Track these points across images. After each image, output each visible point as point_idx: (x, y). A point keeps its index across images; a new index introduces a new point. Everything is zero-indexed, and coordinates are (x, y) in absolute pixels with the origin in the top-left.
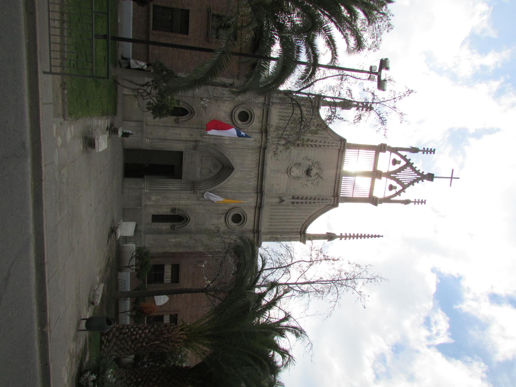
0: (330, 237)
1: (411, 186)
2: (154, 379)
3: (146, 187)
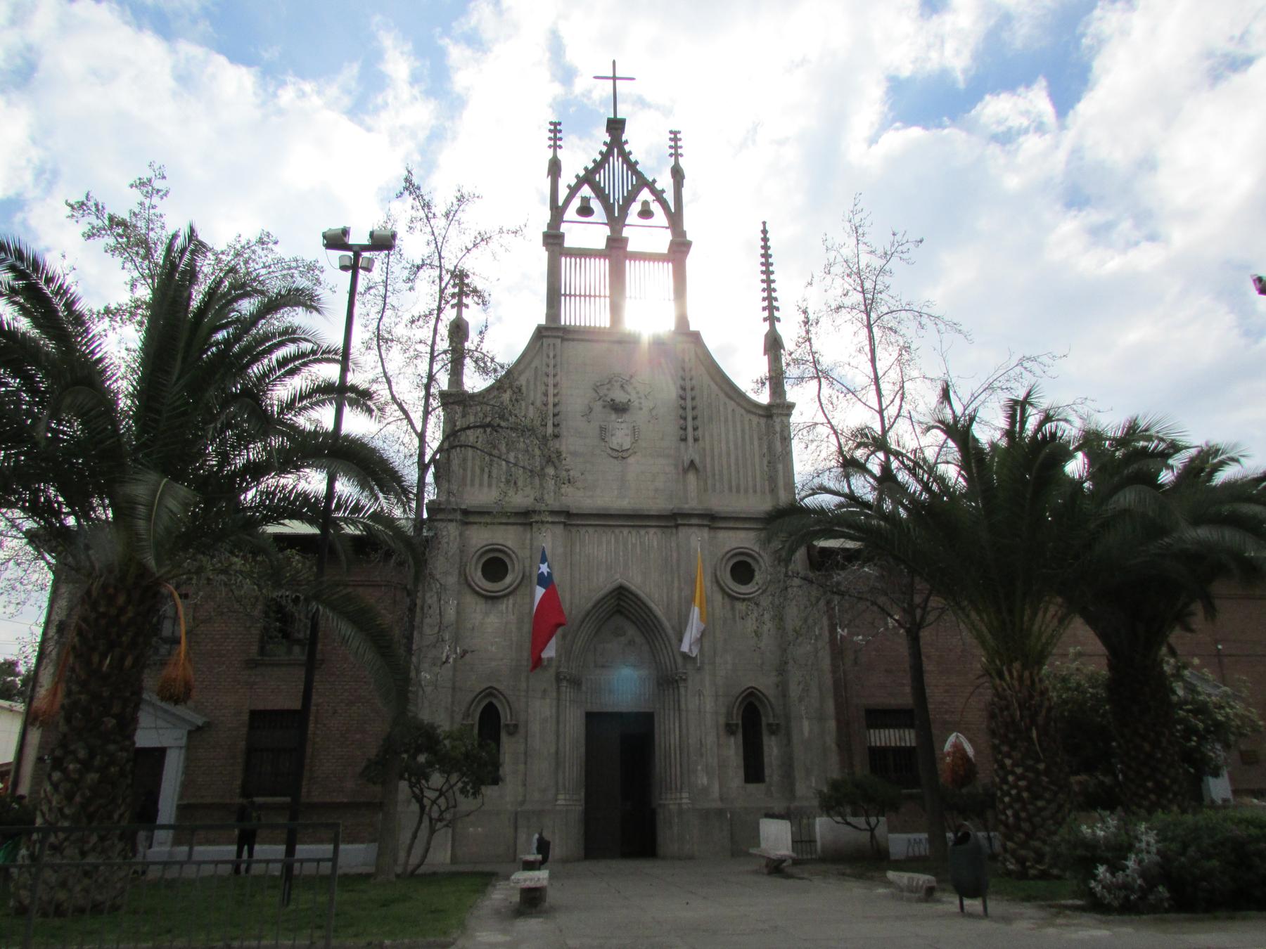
0: (773, 345)
1: (639, 168)
2: (1147, 747)
3: (676, 799)
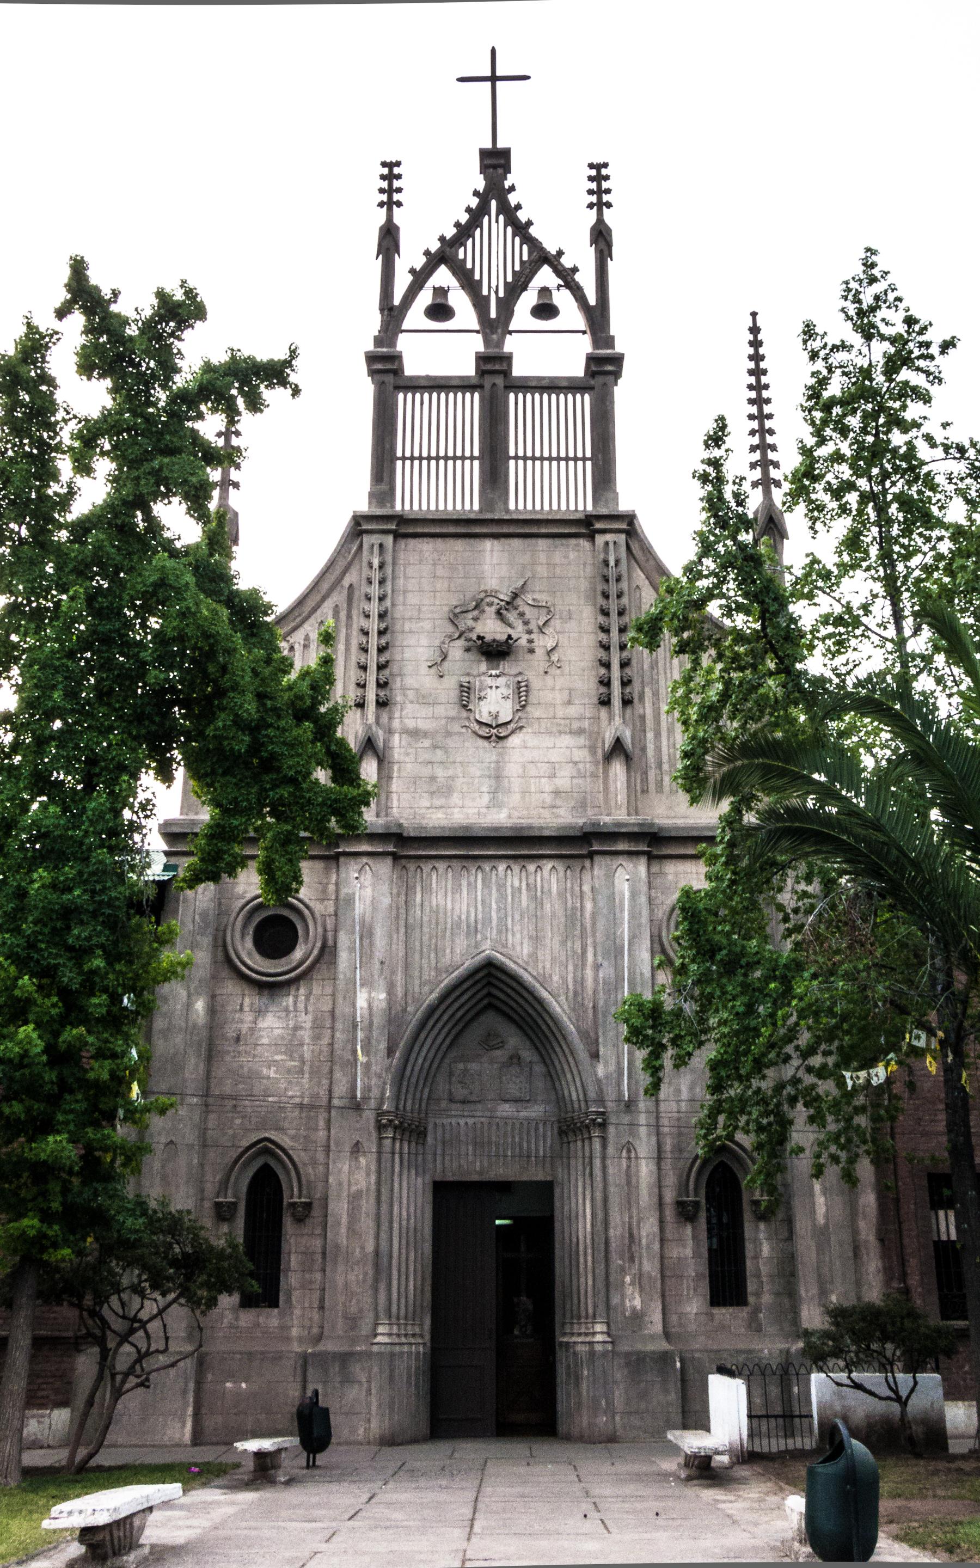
1: (533, 231)
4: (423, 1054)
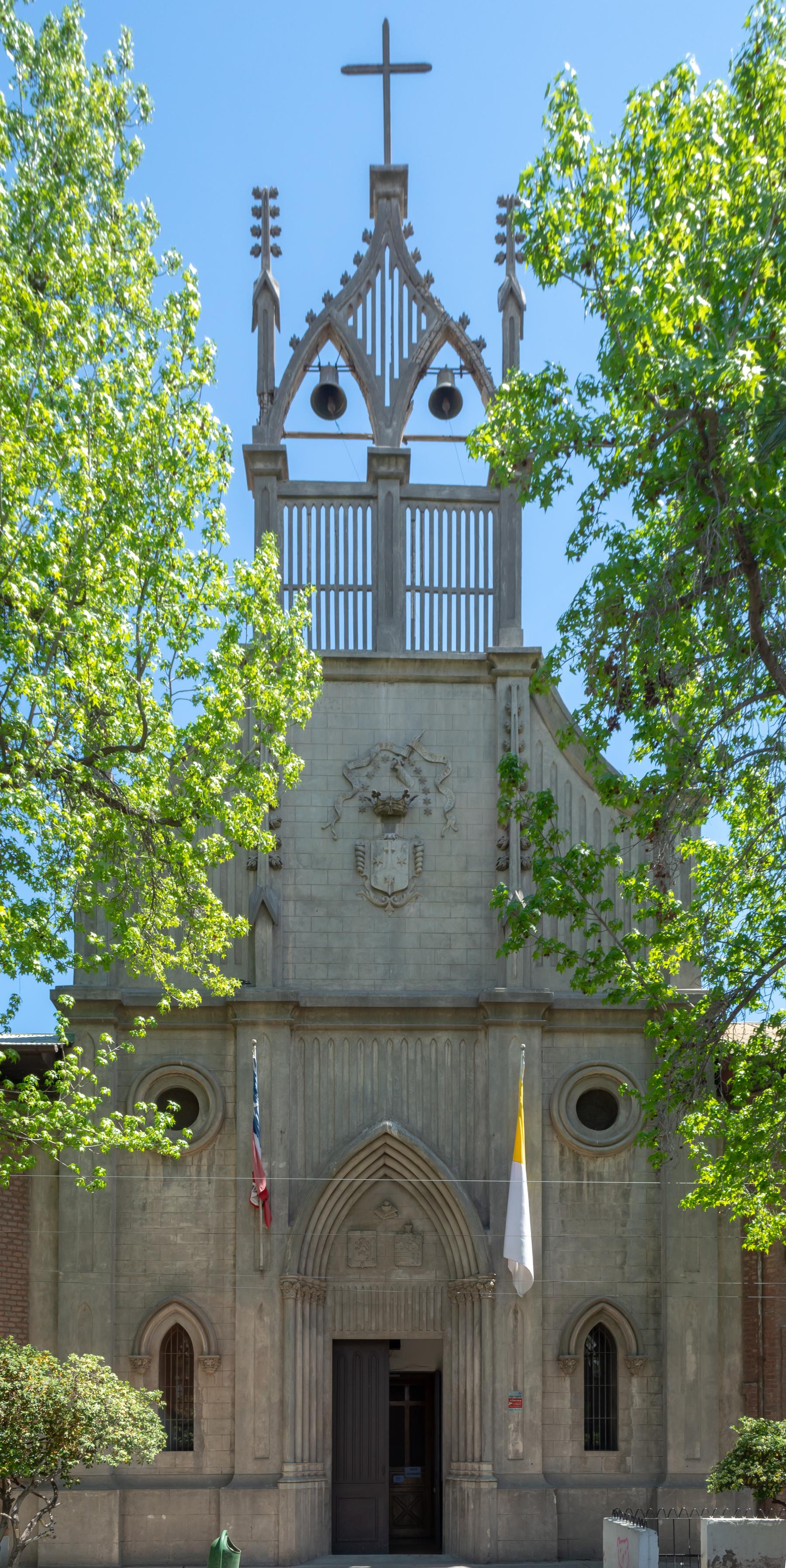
1: (434, 290)
4: (323, 1221)
